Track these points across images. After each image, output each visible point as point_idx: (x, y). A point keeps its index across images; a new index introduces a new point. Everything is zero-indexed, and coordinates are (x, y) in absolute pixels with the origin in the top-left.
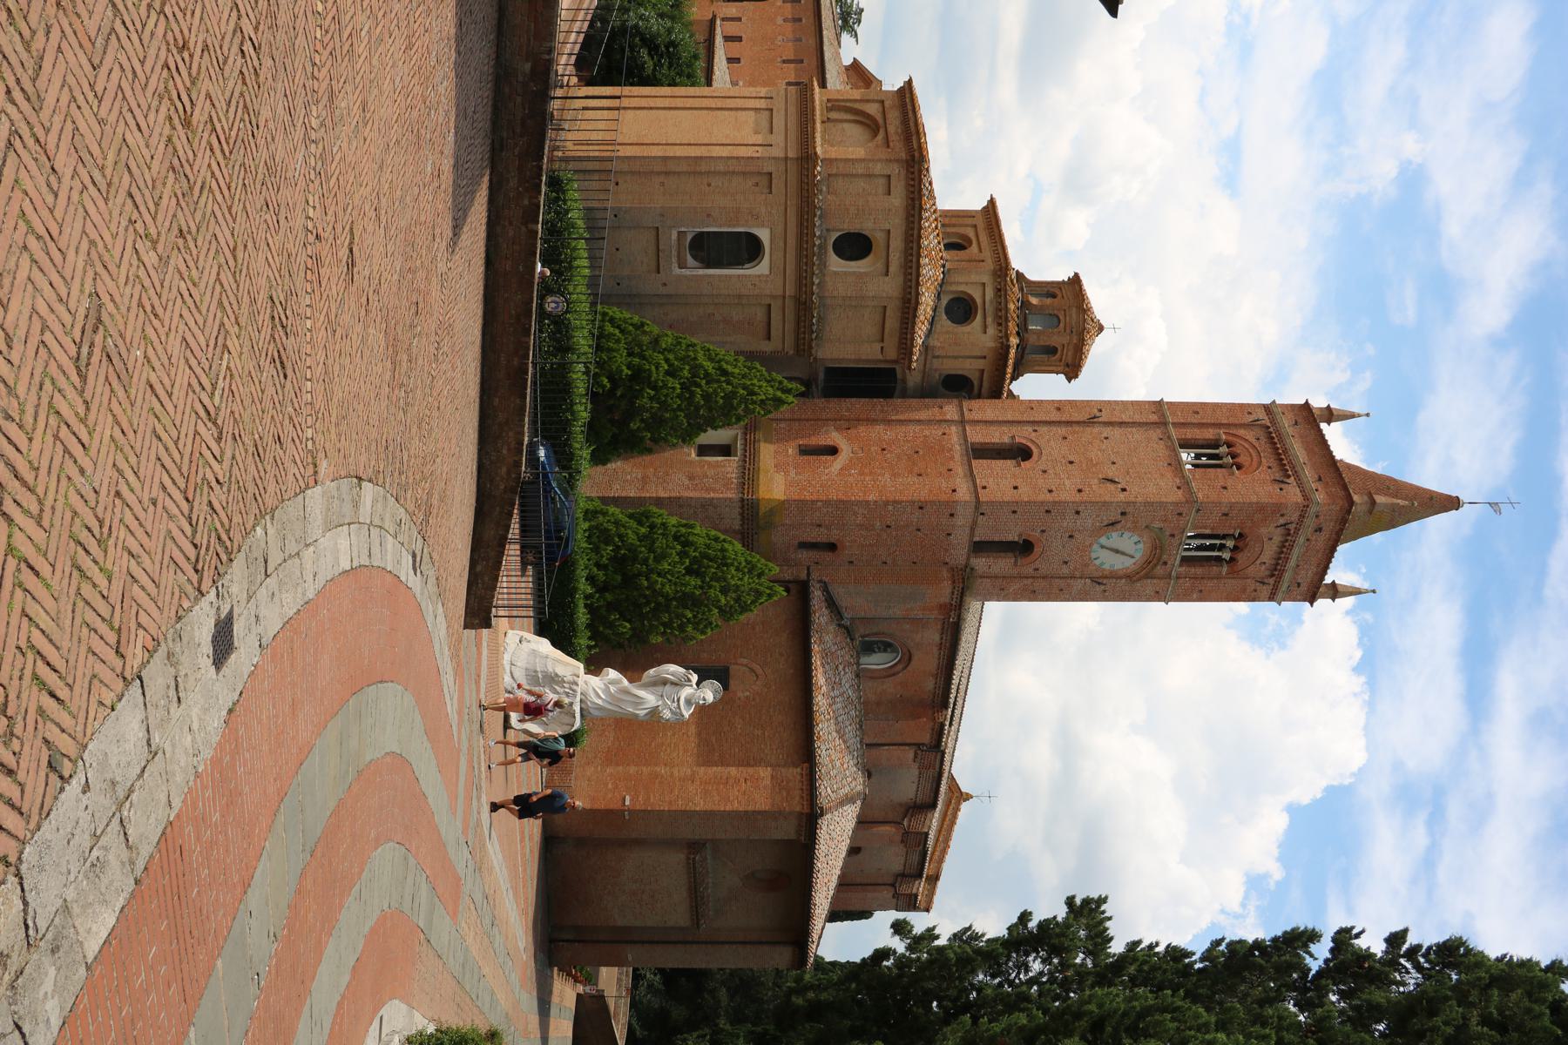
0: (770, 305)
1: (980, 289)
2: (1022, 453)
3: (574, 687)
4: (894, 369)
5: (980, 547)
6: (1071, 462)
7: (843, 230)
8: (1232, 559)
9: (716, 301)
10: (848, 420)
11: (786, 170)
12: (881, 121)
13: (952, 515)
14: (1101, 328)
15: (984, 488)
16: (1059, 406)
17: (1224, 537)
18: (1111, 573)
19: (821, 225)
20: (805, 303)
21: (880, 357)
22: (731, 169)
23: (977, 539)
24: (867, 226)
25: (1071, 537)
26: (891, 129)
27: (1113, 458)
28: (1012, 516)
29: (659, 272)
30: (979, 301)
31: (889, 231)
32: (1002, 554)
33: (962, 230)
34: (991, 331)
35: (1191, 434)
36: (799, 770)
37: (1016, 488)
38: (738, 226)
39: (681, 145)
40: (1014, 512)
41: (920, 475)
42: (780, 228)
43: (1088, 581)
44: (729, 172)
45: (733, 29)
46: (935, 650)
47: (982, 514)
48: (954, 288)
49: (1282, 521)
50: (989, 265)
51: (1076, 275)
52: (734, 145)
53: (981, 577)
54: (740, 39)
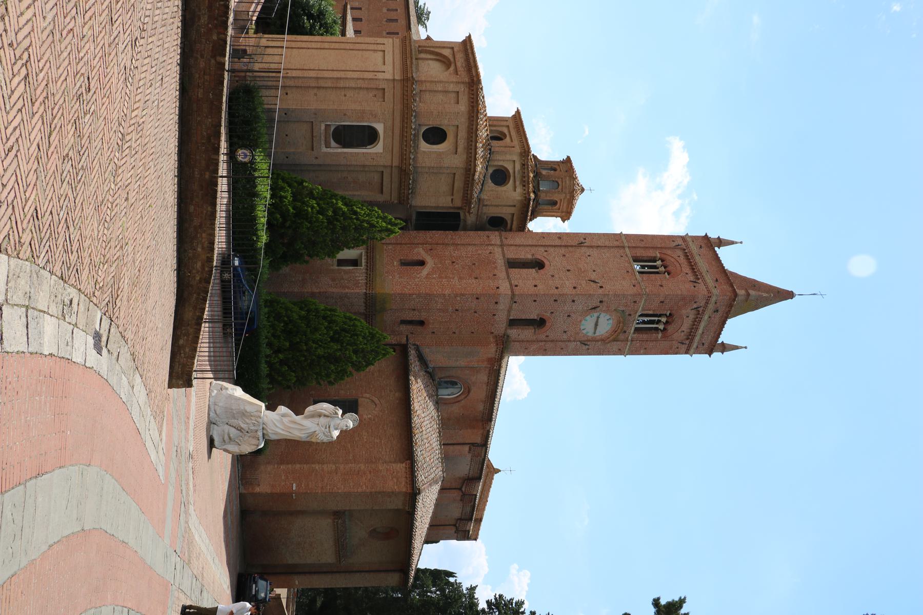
0: (383, 172)
2: (539, 265)
4: (459, 213)
5: (513, 323)
6: (568, 270)
8: (665, 329)
11: (394, 87)
12: (452, 60)
14: (583, 190)
15: (516, 286)
16: (560, 236)
17: (660, 316)
19: (415, 122)
20: (405, 170)
21: (451, 205)
22: (359, 86)
24: (443, 123)
25: (569, 316)
26: (459, 64)
27: (594, 268)
29: (313, 150)
30: (511, 171)
31: (458, 126)
32: (527, 327)
33: (500, 129)
34: (519, 190)
35: (640, 253)
36: (404, 465)
37: (535, 286)
38: (364, 122)
39: (327, 70)
40: (535, 301)
46: (484, 386)
47: (515, 302)
48: (496, 163)
49: (695, 306)
50: (518, 149)
51: (568, 158)
52: (361, 71)
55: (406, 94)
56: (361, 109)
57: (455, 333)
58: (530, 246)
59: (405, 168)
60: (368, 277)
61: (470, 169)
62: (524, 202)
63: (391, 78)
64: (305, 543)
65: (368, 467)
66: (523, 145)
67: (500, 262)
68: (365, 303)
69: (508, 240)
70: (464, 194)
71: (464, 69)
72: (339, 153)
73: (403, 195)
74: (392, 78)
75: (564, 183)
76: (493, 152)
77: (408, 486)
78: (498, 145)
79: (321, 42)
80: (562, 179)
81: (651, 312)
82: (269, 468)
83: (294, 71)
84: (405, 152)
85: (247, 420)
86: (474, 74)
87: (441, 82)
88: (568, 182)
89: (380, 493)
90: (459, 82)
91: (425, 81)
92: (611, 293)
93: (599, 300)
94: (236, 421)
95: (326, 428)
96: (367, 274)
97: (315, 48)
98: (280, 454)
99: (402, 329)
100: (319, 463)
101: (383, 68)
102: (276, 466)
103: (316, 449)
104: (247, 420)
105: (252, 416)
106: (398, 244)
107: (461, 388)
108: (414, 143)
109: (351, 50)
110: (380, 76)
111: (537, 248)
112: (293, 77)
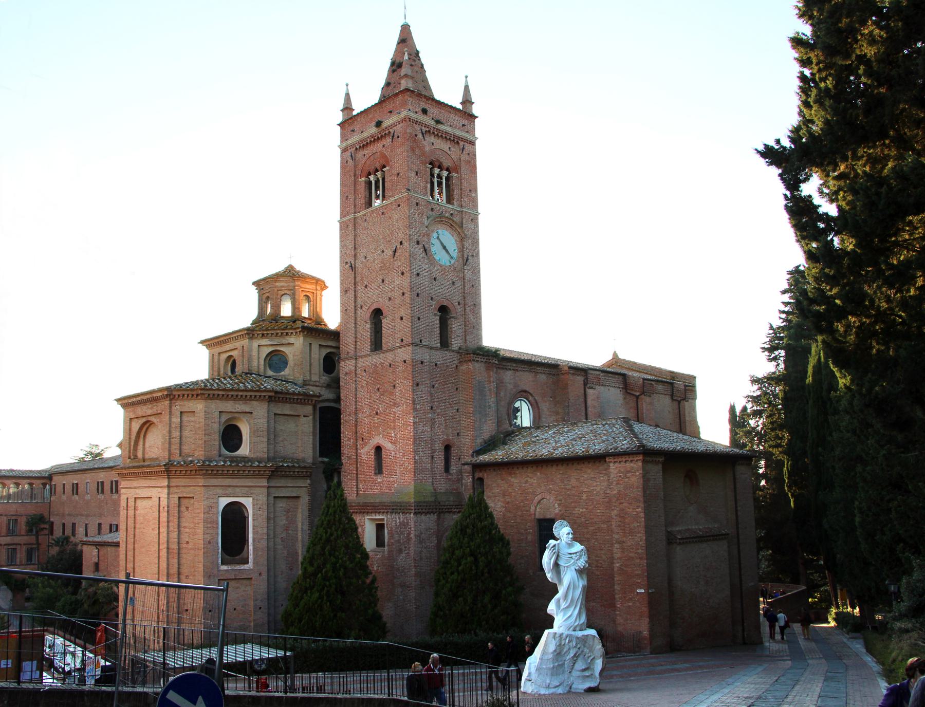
0: (275, 497)
3: (564, 636)
4: (320, 408)
5: (445, 343)
6: (383, 281)
8: (447, 170)
9: (272, 536)
10: (357, 440)
11: (177, 486)
12: (144, 420)
13: (422, 363)
15: (402, 340)
16: (344, 291)
17: (432, 175)
18: (459, 252)
19: (216, 461)
20: (272, 471)
21: (311, 417)
22: (176, 527)
23: (439, 345)
24: (216, 429)
26: (149, 412)
29: (251, 578)
30: (271, 349)
32: (449, 327)
33: (222, 363)
34: (292, 340)
35: (361, 201)
36: (611, 465)
37: (402, 318)
38: (217, 521)
39: (159, 564)
40: (419, 319)
42: (219, 490)
45: (93, 530)
46: (518, 374)
47: (421, 341)
48: (262, 367)
49: (420, 136)
50: (245, 342)
51: (254, 283)
52: (159, 525)
53: (466, 342)
54: (100, 525)
57: (458, 410)
59: (269, 471)
62: (305, 333)
63: (166, 490)
65: (615, 506)
67: (377, 358)
68: (426, 514)
73: (300, 473)
74: (167, 489)
76: (249, 370)
77: (636, 459)
78: (241, 364)
81: (429, 186)
82: (620, 620)
84: (252, 472)
85: (565, 650)
86: (160, 394)
87: (170, 432)
88: (282, 284)
90: (170, 412)
91: (170, 451)
95: (572, 558)
99: (455, 471)
100: (613, 563)
102: (618, 612)
103: (597, 566)
104: (565, 650)
105: (560, 644)
106: (357, 478)
110: (164, 503)
111: (359, 319)
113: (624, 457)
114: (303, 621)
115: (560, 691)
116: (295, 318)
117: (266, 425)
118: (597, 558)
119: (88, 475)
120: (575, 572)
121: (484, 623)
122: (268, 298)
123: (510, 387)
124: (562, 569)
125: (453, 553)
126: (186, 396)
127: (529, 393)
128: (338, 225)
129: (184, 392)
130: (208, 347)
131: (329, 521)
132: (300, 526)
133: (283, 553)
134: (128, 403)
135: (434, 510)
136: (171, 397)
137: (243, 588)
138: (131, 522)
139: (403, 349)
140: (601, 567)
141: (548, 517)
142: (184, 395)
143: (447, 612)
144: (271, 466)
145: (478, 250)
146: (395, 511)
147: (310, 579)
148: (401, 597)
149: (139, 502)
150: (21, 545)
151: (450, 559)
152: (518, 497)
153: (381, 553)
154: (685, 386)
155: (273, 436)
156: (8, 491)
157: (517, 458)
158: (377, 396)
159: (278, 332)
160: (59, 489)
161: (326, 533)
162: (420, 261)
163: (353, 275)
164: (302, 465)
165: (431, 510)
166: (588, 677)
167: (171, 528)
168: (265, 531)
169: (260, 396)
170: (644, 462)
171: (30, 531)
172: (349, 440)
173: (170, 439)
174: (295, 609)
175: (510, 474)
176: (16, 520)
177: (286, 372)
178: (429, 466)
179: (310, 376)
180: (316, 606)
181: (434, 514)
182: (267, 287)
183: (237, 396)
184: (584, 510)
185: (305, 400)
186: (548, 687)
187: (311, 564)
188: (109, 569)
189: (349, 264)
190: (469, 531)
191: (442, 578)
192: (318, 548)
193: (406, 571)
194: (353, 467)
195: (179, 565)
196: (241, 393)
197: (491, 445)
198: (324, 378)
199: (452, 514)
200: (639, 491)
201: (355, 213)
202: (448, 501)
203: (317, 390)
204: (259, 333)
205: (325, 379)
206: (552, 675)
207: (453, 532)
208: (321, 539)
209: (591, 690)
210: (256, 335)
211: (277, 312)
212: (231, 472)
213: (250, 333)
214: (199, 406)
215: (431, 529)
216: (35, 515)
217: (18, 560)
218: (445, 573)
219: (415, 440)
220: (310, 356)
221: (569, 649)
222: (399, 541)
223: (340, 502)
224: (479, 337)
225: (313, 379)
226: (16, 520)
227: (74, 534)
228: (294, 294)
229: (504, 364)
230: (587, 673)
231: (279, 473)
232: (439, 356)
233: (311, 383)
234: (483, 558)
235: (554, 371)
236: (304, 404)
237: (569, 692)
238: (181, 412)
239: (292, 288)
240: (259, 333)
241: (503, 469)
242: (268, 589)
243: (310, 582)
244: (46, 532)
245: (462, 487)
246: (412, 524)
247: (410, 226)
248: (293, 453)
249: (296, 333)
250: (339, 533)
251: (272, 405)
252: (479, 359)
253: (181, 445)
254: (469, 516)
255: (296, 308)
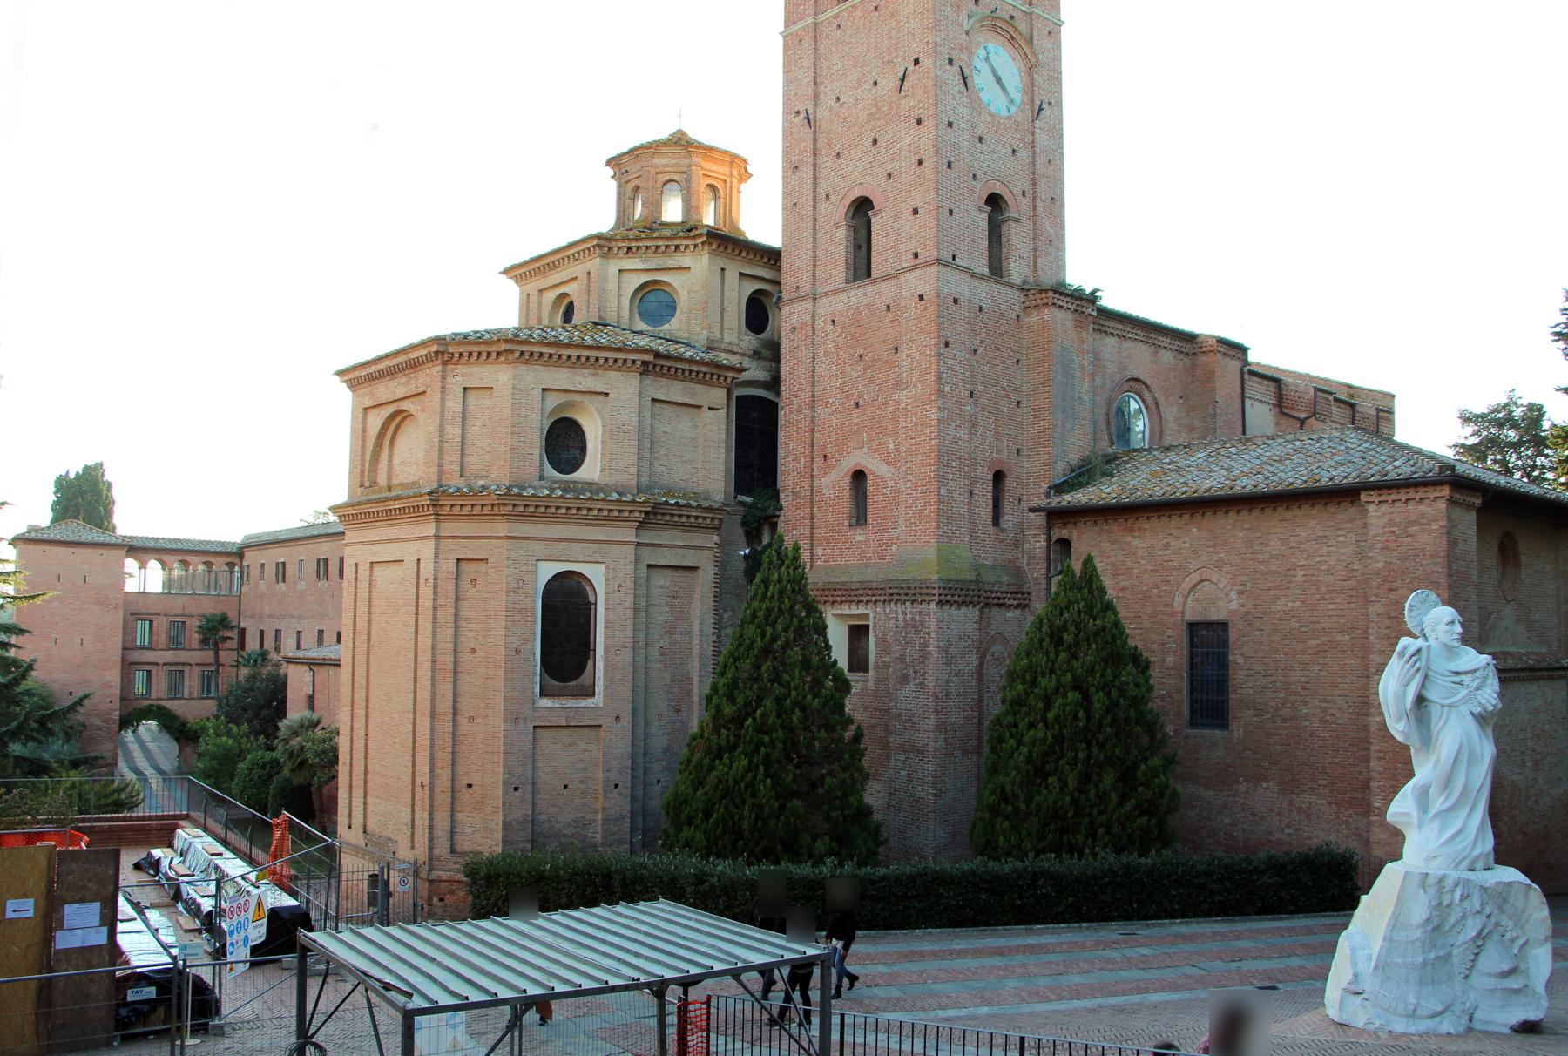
0: (649, 566)
1: (626, 276)
2: (862, 207)
3: (1449, 882)
4: (737, 397)
5: (997, 269)
6: (875, 141)
7: (541, 461)
9: (642, 643)
10: (812, 459)
12: (391, 409)
13: (956, 301)
15: (916, 255)
16: (791, 168)
18: (1025, 93)
19: (534, 488)
20: (647, 513)
21: (723, 412)
22: (452, 619)
23: (986, 271)
25: (981, 139)
26: (401, 392)
27: (868, 86)
28: (956, 215)
29: (600, 726)
30: (644, 278)
32: (1004, 239)
33: (546, 309)
34: (685, 260)
36: (1371, 508)
37: (916, 212)
38: (534, 608)
39: (415, 692)
40: (951, 212)
41: (896, 349)
42: (538, 548)
43: (1037, 123)
44: (456, 621)
45: (309, 639)
46: (1127, 344)
47: (954, 258)
48: (626, 312)
50: (594, 263)
51: (609, 162)
52: (417, 614)
53: (1035, 270)
54: (321, 632)
55: (469, 508)
56: (504, 613)
57: (1019, 402)
58: (814, 234)
59: (641, 512)
60: (898, 597)
61: (644, 363)
62: (714, 247)
63: (432, 544)
64: (1534, 751)
65: (1377, 595)
66: (584, 251)
67: (861, 295)
68: (960, 604)
69: (801, 284)
70: (699, 382)
71: (411, 379)
72: (606, 666)
73: (700, 520)
74: (433, 541)
75: (667, 169)
76: (600, 317)
77: (1432, 495)
78: (584, 307)
79: (352, 706)
80: (657, 173)
83: (417, 768)
84: (605, 513)
85: (1452, 919)
86: (423, 352)
87: (442, 428)
88: (665, 161)
89: (1449, 566)
90: (443, 387)
91: (440, 466)
92: (931, 38)
93: (948, 67)
94: (1455, 952)
95: (1461, 683)
96: (890, 601)
97: (367, 721)
98: (1333, 806)
99: (1010, 524)
101: (410, 564)
102: (1375, 818)
103: (1323, 721)
104: (1452, 919)
105: (1440, 904)
106: (812, 534)
107: (1130, 397)
108: (584, 491)
109: (369, 639)
110: (427, 570)
111: (821, 220)
112: (432, 770)
113: (1403, 491)
114: (714, 816)
115: (1446, 1026)
116: (689, 229)
117: (635, 419)
118: (1325, 705)
119: (301, 548)
120: (1470, 719)
121: (1101, 831)
122: (637, 188)
123: (1112, 368)
124: (1434, 710)
125: (1034, 683)
126: (475, 355)
127: (1147, 386)
128: (780, 41)
129: (471, 348)
130: (519, 279)
131: (768, 610)
132: (696, 627)
133: (664, 678)
134: (359, 377)
135: (976, 599)
136: (446, 357)
137: (583, 746)
138: (362, 610)
139: (918, 272)
140: (1333, 722)
141: (1213, 617)
142: (470, 354)
143: (1023, 806)
144: (644, 502)
145: (1060, 92)
146: (895, 597)
147: (729, 730)
148: (902, 772)
149: (377, 569)
150: (191, 665)
151: (1028, 695)
152: (1145, 576)
153: (860, 684)
154: (1378, 410)
155: (648, 445)
156: (170, 575)
157: (1151, 496)
158: (857, 371)
159: (660, 243)
160: (255, 572)
161: (763, 635)
162: (954, 99)
163: (811, 136)
164: (705, 504)
165: (969, 599)
166: (1516, 991)
167: (441, 619)
168: (629, 633)
169: (625, 361)
170: (1452, 502)
171: (204, 642)
172: (796, 459)
173: (441, 441)
174: (695, 791)
175: (1131, 530)
176: (184, 623)
177: (673, 326)
178: (964, 510)
179: (722, 334)
180: (743, 784)
181: (974, 606)
182: (634, 168)
183: (579, 358)
184: (1298, 604)
185: (712, 375)
186: (1412, 1015)
187: (731, 698)
188: (331, 706)
189: (804, 115)
190: (1068, 638)
191: (1007, 734)
192: (747, 665)
193: (916, 719)
194: (803, 514)
195: (455, 694)
196: (586, 353)
197: (1082, 475)
198: (747, 338)
199: (1004, 609)
200: (1436, 564)
201: (816, 14)
202: (1000, 583)
203: (735, 360)
204: (620, 244)
205: (750, 341)
206: (1421, 983)
207: (1031, 640)
208: (750, 647)
209: (1528, 1028)
210: (615, 250)
211: (655, 215)
212: (563, 511)
213: (602, 244)
214: (501, 376)
215: (969, 637)
216: (214, 615)
217: (186, 691)
218: (1016, 726)
219: (940, 455)
220: (722, 293)
221: (1463, 917)
222: (902, 659)
223: (792, 573)
224: (1061, 266)
225: (727, 339)
226: (184, 623)
227: (278, 649)
228: (688, 181)
229: (1102, 322)
230: (1513, 983)
231: (659, 517)
232: (985, 292)
233: (723, 346)
234: (1101, 694)
235: (1187, 347)
236: (710, 384)
237: (1470, 1030)
238: (465, 389)
239: (685, 169)
240: (620, 244)
241: (1116, 520)
242: (632, 749)
243: (728, 736)
244: (234, 644)
245: (1023, 557)
246: (932, 624)
247: (936, 27)
248: (685, 481)
249: (696, 246)
250: (791, 635)
251: (649, 382)
252: (1064, 304)
253: (462, 454)
254: (1068, 608)
255: (689, 206)
